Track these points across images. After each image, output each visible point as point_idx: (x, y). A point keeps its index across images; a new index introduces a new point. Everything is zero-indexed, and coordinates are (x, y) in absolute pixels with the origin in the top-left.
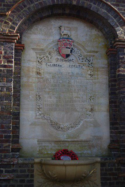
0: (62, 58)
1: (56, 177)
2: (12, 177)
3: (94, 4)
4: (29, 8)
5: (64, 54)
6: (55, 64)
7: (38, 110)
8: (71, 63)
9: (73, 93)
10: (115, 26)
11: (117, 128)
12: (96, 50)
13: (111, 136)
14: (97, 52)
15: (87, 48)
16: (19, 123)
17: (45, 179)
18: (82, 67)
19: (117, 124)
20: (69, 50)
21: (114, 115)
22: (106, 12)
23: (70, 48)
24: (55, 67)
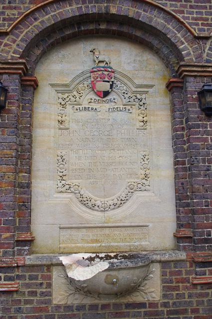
0: (98, 98)
1: (86, 287)
3: (144, 11)
4: (42, 22)
5: (101, 91)
6: (87, 106)
8: (112, 105)
10: (178, 44)
11: (188, 205)
14: (151, 86)
21: (182, 184)
22: (164, 22)
23: (108, 82)
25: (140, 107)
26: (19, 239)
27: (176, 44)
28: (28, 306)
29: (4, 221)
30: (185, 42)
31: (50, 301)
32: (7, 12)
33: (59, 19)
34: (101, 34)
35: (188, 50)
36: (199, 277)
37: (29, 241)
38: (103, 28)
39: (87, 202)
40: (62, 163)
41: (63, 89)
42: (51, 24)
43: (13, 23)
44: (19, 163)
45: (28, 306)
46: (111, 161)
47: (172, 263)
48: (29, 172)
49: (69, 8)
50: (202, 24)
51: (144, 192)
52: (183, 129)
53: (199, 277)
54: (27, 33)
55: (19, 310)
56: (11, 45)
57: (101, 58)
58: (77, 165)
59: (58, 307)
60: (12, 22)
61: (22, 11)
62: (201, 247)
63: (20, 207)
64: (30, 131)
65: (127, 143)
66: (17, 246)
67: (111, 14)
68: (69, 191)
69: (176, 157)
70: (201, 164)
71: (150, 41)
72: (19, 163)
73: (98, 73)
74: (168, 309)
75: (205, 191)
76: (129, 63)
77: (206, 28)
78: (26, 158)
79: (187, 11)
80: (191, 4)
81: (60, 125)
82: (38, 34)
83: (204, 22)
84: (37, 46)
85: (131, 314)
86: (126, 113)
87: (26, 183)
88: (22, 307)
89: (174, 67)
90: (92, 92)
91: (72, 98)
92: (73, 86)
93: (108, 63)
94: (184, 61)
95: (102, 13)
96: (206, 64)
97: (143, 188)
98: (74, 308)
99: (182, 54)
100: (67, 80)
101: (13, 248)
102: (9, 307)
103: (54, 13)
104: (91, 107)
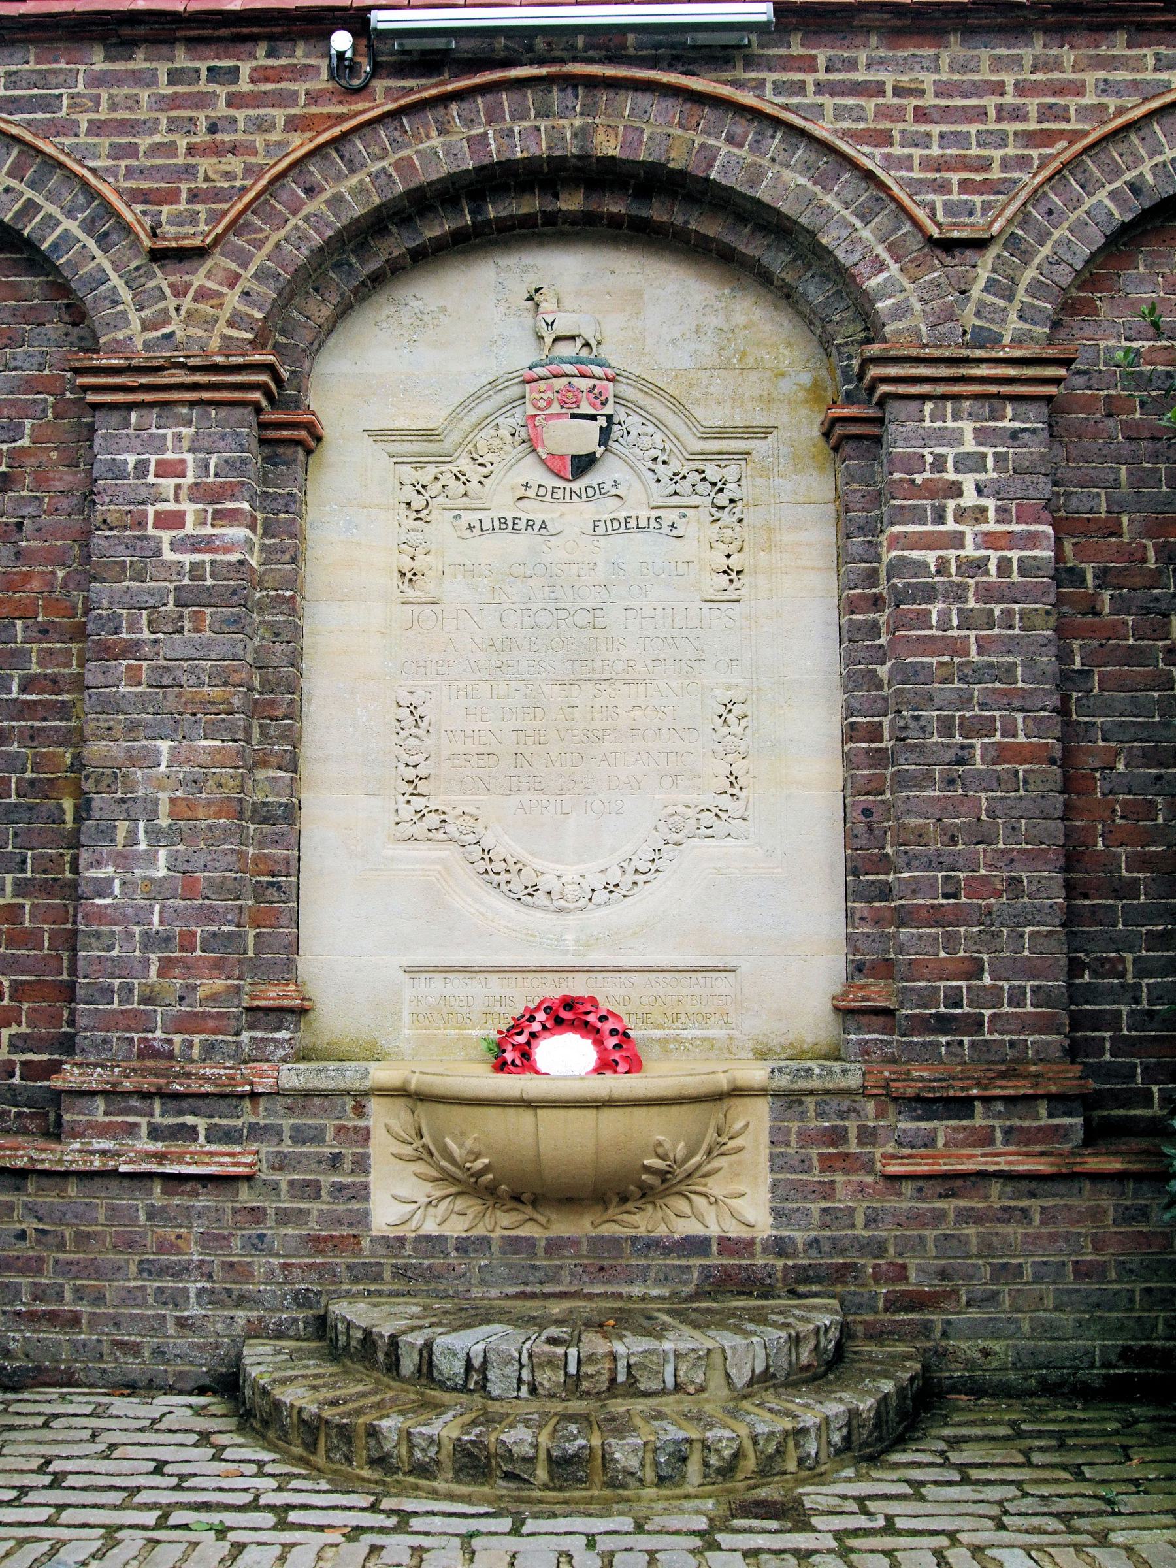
0: (551, 481)
1: (487, 1169)
2: (245, 1165)
3: (730, 140)
4: (336, 202)
5: (562, 456)
6: (509, 516)
7: (409, 789)
8: (608, 508)
9: (619, 685)
10: (864, 270)
11: (885, 892)
12: (760, 420)
13: (850, 939)
14: (765, 432)
15: (698, 412)
16: (293, 867)
17: (437, 1180)
18: (673, 526)
19: (884, 863)
20: (593, 428)
21: (867, 812)
22: (809, 185)
23: (593, 418)
24: (509, 537)
25: (717, 515)
26: (256, 1003)
27: (854, 271)
28: (290, 1231)
29: (203, 939)
30: (889, 261)
31: (363, 1218)
32: (205, 164)
33: (400, 188)
34: (567, 227)
35: (903, 297)
36: (908, 1151)
37: (290, 1010)
38: (572, 208)
39: (505, 876)
40: (414, 731)
41: (421, 447)
42: (371, 206)
43: (228, 211)
44: (256, 731)
45: (290, 1231)
46: (598, 724)
47: (810, 1101)
48: (292, 765)
49: (436, 141)
50: (965, 185)
51: (722, 842)
52: (875, 604)
53: (908, 1151)
54: (278, 246)
55: (258, 1244)
56: (222, 295)
57: (561, 329)
58: (469, 741)
59: (396, 1244)
60: (226, 206)
61: (259, 160)
62: (924, 1045)
63: (259, 891)
64: (294, 611)
65: (662, 656)
66: (251, 1028)
67: (598, 159)
68: (440, 835)
69: (849, 711)
70: (935, 739)
71: (757, 254)
72: (256, 731)
73: (551, 387)
74: (790, 1263)
75: (946, 839)
76: (673, 341)
77: (977, 199)
78: (280, 713)
79: (903, 132)
80: (920, 103)
81: (406, 587)
82: (321, 249)
83: (972, 176)
84: (317, 290)
85: (653, 1274)
86: (662, 539)
87: (281, 805)
88: (270, 1232)
89: (850, 357)
90: (531, 459)
91: (452, 483)
92: (455, 437)
93: (593, 343)
94: (884, 340)
95: (564, 158)
96: (965, 352)
97: (720, 827)
98: (450, 1246)
99: (876, 312)
100: (430, 416)
101: (237, 1034)
102: (226, 1232)
103: (380, 165)
104: (524, 517)
